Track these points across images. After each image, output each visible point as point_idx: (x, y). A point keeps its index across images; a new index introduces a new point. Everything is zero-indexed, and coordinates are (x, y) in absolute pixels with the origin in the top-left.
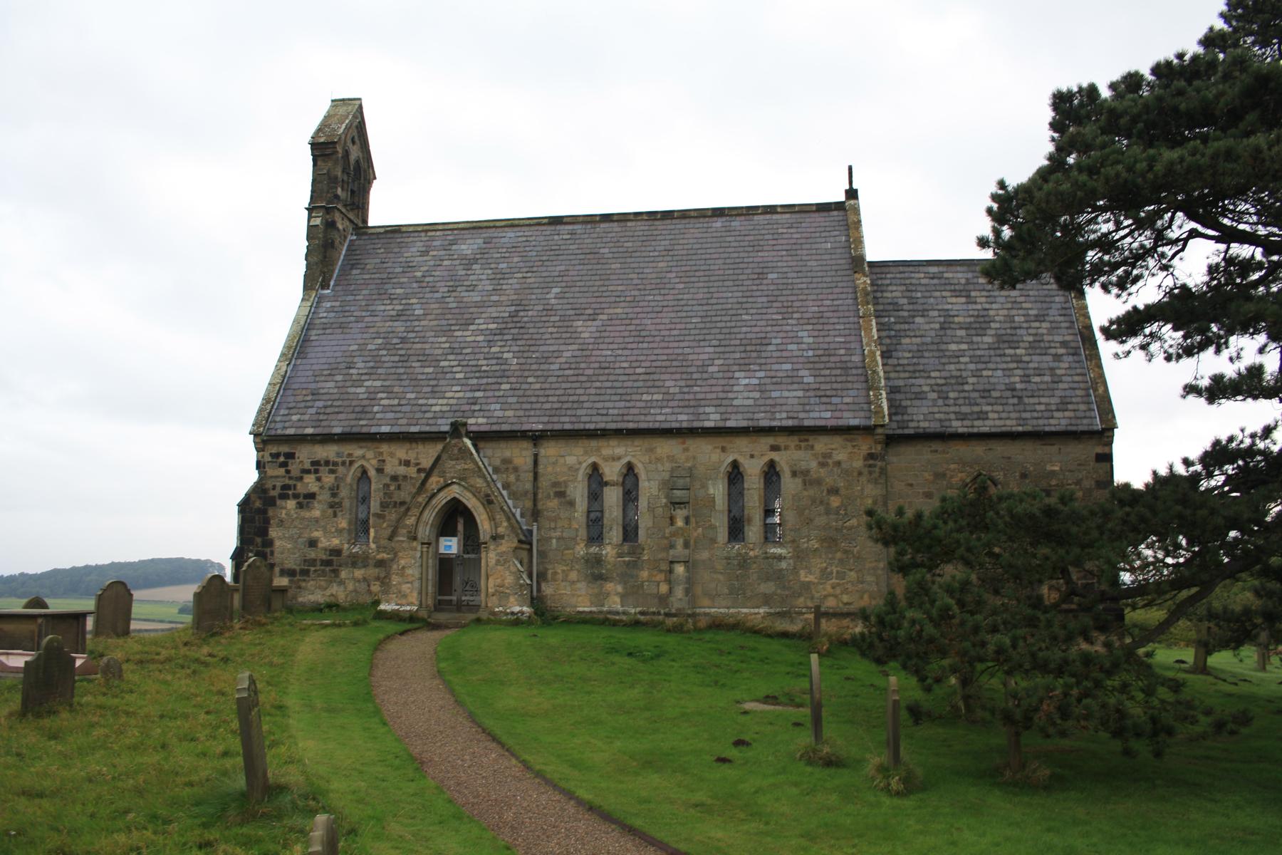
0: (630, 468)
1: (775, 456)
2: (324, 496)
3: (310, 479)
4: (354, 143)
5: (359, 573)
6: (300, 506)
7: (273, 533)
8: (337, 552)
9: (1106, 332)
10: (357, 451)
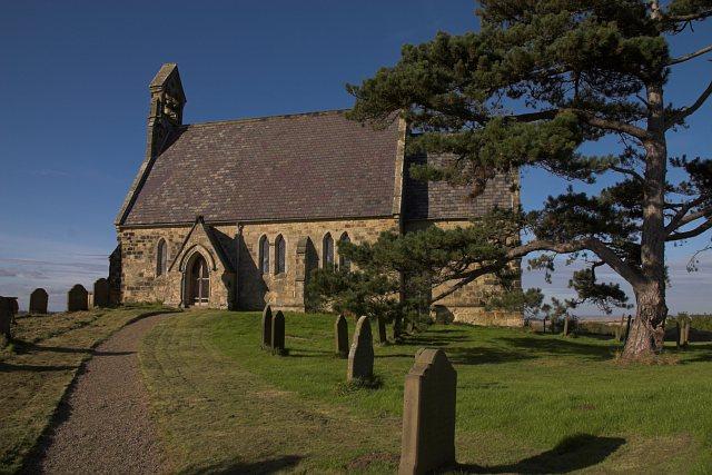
0: (280, 237)
1: (347, 230)
2: (146, 253)
3: (140, 245)
4: (173, 85)
5: (161, 289)
6: (136, 257)
7: (124, 270)
8: (152, 279)
9: (672, 160)
10: (161, 231)
